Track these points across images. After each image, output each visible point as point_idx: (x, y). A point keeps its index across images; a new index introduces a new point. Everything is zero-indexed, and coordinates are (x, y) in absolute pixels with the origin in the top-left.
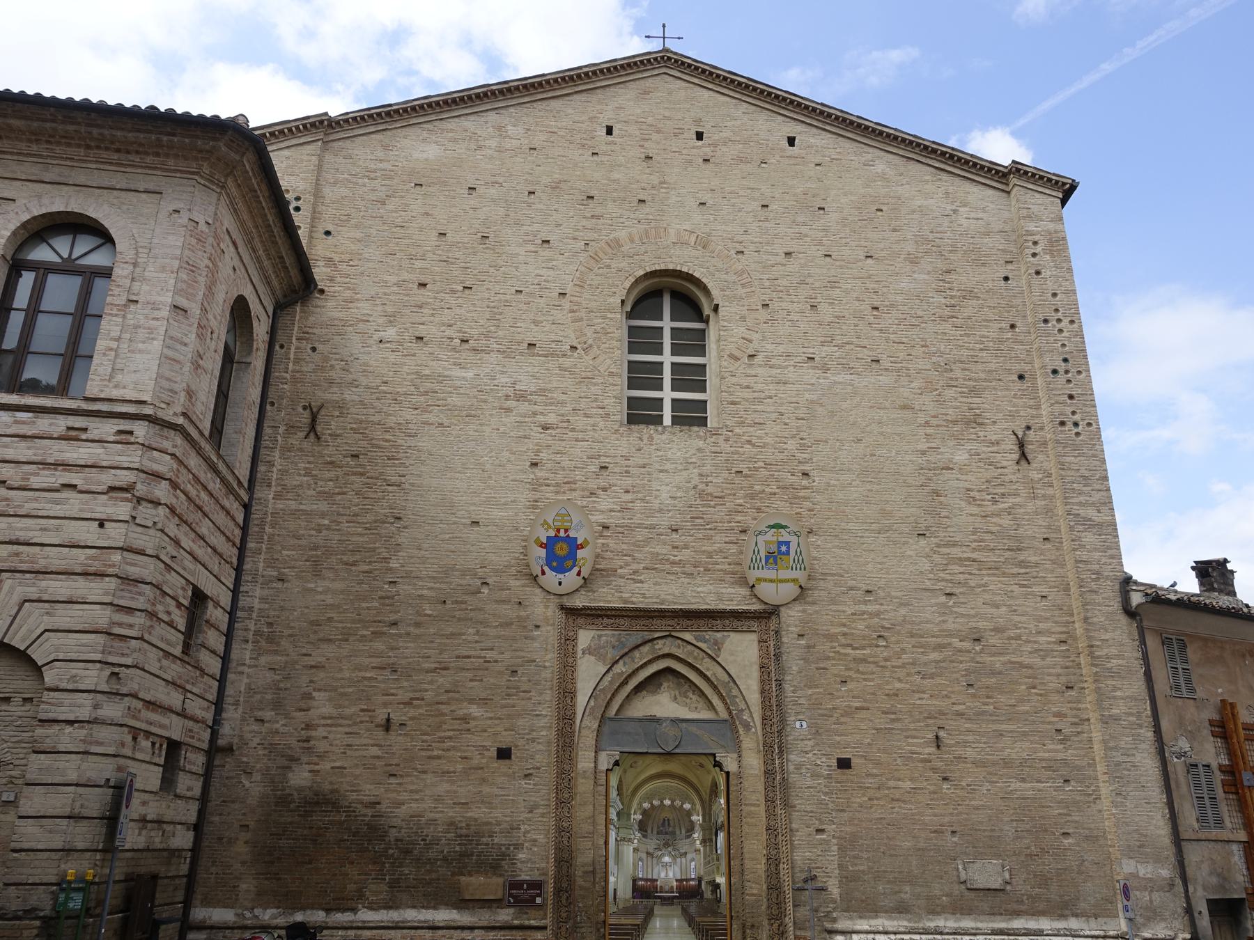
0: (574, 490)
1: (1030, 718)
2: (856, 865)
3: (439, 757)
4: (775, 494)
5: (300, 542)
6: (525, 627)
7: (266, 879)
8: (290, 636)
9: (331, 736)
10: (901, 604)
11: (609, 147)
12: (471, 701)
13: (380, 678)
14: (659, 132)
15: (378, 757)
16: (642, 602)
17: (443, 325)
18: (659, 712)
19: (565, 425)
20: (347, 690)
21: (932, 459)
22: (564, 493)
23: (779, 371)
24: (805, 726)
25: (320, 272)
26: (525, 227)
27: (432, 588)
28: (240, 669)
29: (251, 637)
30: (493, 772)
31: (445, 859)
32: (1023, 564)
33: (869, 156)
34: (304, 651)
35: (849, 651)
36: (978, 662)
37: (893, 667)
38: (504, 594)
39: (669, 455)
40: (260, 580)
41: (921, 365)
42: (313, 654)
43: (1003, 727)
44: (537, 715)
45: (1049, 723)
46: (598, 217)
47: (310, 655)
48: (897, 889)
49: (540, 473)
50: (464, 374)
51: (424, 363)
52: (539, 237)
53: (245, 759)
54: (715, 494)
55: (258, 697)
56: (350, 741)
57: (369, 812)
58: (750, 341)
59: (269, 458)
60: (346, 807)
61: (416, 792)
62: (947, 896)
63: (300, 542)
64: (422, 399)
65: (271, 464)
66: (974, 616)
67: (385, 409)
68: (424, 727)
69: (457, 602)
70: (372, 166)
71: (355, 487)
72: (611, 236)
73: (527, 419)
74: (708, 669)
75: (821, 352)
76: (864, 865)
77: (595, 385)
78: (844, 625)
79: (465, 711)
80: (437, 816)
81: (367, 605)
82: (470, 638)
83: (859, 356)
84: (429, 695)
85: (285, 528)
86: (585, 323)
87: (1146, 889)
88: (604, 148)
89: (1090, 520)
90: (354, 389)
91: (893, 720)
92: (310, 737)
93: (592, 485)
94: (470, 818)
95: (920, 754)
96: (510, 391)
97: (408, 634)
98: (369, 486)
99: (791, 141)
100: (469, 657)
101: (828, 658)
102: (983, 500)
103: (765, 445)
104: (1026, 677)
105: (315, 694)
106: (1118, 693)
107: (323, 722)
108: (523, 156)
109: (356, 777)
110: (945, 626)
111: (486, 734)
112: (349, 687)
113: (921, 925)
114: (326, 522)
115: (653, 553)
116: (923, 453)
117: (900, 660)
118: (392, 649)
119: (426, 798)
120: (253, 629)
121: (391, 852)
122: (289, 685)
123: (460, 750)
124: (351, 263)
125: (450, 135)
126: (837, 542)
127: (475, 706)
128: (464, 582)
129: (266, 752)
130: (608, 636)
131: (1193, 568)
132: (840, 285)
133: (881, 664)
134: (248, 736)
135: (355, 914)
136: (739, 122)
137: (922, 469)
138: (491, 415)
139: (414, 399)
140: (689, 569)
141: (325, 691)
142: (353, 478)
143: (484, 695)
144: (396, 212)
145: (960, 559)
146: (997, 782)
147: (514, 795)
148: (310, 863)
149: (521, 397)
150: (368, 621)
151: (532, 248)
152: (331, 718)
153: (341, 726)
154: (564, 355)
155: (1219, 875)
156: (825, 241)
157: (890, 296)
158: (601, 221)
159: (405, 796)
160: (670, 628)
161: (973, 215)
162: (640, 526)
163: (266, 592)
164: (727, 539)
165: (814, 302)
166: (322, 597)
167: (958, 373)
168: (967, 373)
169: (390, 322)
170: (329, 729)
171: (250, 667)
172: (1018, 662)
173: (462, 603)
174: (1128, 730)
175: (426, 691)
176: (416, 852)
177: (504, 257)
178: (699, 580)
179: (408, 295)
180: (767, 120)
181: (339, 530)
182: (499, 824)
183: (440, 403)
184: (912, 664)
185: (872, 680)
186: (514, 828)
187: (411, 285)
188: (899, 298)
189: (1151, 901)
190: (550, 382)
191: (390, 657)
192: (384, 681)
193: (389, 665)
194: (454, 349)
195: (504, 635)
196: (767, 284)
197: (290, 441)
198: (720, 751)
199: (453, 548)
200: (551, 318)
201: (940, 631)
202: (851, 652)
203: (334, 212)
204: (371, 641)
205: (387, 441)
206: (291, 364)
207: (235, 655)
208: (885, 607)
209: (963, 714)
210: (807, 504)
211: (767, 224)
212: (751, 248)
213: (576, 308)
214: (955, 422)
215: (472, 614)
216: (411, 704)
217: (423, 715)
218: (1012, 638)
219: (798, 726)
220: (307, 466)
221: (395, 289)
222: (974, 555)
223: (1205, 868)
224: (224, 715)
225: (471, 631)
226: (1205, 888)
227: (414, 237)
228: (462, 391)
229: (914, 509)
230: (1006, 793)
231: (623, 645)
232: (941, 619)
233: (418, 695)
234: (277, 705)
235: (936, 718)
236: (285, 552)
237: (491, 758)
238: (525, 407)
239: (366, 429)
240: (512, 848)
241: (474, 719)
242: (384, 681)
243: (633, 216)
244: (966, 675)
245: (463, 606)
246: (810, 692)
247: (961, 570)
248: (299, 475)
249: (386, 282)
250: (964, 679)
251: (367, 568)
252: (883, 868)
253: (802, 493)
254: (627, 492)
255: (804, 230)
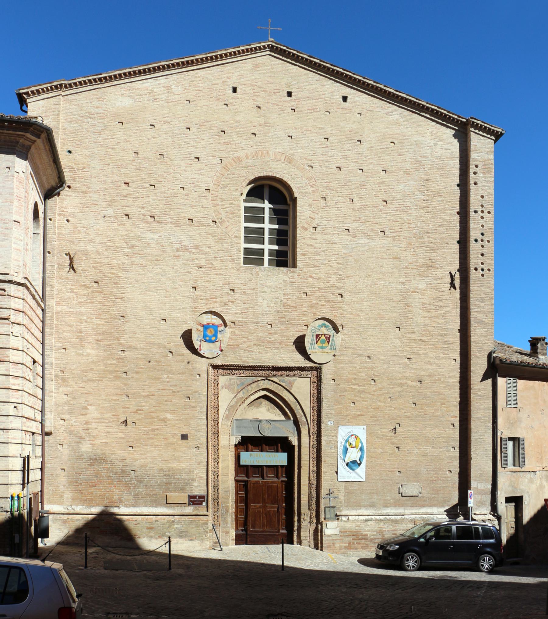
0: (216, 302)
1: (440, 419)
2: (353, 487)
3: (152, 438)
4: (323, 305)
5: (72, 329)
6: (192, 375)
7: (75, 493)
8: (73, 377)
9: (99, 428)
10: (384, 363)
11: (234, 100)
12: (167, 411)
13: (121, 399)
14: (265, 91)
15: (123, 438)
16: (252, 362)
17: (139, 207)
18: (260, 417)
19: (210, 266)
20: (104, 405)
21: (407, 287)
22: (211, 304)
23: (329, 236)
24: (333, 424)
25: (67, 175)
26: (184, 149)
27: (143, 354)
28: (51, 394)
29: (53, 378)
30: (180, 446)
31: (159, 485)
32: (446, 342)
33: (390, 109)
34: (81, 386)
35: (357, 387)
36: (419, 392)
37: (378, 395)
38: (181, 358)
39: (268, 284)
40: (54, 348)
41: (406, 234)
42: (86, 387)
43: (428, 423)
44: (200, 419)
45: (448, 421)
46: (227, 144)
47: (84, 388)
48: (370, 497)
49: (198, 293)
50: (153, 236)
51: (130, 229)
52: (192, 155)
53: (58, 438)
54: (292, 305)
55: (61, 408)
56: (109, 430)
57: (121, 464)
58: (314, 219)
59: (51, 283)
60: (110, 461)
61: (143, 454)
62: (393, 499)
63: (72, 329)
64: (130, 250)
65: (52, 286)
66: (419, 369)
67: (110, 256)
68: (144, 424)
69: (156, 361)
70: (92, 110)
71: (98, 299)
72: (236, 155)
73: (189, 262)
74: (286, 396)
75: (352, 226)
76: (356, 487)
77: (226, 243)
78: (355, 374)
79: (164, 416)
80: (154, 465)
81: (110, 362)
82: (164, 380)
83: (374, 228)
84: (146, 408)
85: (63, 321)
86: (220, 207)
87: (480, 494)
88: (231, 101)
89: (482, 320)
90: (92, 244)
91: (376, 420)
92: (89, 428)
93: (225, 299)
94: (170, 467)
95: (387, 436)
96: (179, 246)
97: (133, 377)
98: (106, 299)
99: (345, 99)
100: (164, 390)
101: (346, 391)
102: (430, 309)
103: (319, 278)
104: (441, 399)
105: (88, 407)
106: (482, 407)
107: (94, 421)
108: (182, 105)
109: (113, 447)
110: (405, 374)
111: (175, 427)
112: (105, 403)
113: (380, 512)
114: (85, 318)
115: (258, 336)
116: (403, 283)
117: (381, 392)
118: (126, 385)
119: (148, 457)
120: (54, 374)
121: (133, 482)
122: (75, 403)
123: (163, 435)
124: (84, 170)
125: (138, 91)
126: (354, 331)
127: (169, 414)
128: (159, 351)
129: (68, 435)
130: (235, 380)
131: (529, 341)
132: (366, 187)
133: (372, 393)
134: (58, 427)
135: (119, 509)
136: (314, 86)
137: (401, 292)
138: (169, 260)
139: (126, 250)
140: (277, 345)
141: (94, 405)
142: (97, 294)
143: (173, 409)
144: (108, 139)
145: (416, 340)
146: (422, 449)
147: (190, 456)
148: (95, 486)
149: (185, 250)
150: (111, 371)
151: (189, 162)
152: (98, 419)
153: (103, 423)
154: (209, 226)
155: (513, 487)
156: (360, 161)
157: (394, 194)
158: (229, 146)
159: (137, 457)
160: (267, 376)
161: (445, 147)
162: (251, 322)
163: (58, 355)
164: (297, 330)
165: (351, 197)
166: (86, 358)
167: (426, 239)
168: (430, 239)
169: (110, 205)
170: (97, 424)
171: (55, 393)
172: (437, 392)
173: (159, 362)
174: (483, 424)
175: (144, 406)
176: (145, 482)
177: (173, 167)
178: (282, 351)
179: (118, 189)
180: (330, 85)
181: (92, 322)
182: (183, 469)
183: (141, 252)
184: (387, 393)
185: (367, 401)
186: (191, 471)
187: (119, 184)
188: (398, 196)
189: (481, 499)
190: (201, 242)
191: (124, 389)
192: (122, 401)
193: (124, 393)
194: (146, 222)
195: (181, 379)
196: (325, 185)
197: (61, 273)
198: (291, 435)
199: (152, 333)
200: (200, 204)
201: (402, 377)
202: (358, 387)
203: (72, 139)
204: (114, 381)
205: (113, 274)
206: (56, 230)
207: (47, 387)
208: (376, 365)
209: (409, 417)
210: (340, 311)
211: (326, 150)
212: (317, 164)
213: (215, 198)
214: (421, 267)
215: (165, 368)
216: (137, 412)
217: (143, 418)
218: (437, 380)
219: (329, 424)
220: (71, 287)
221: (111, 186)
222: (423, 338)
223: (507, 484)
224: (46, 417)
225: (165, 376)
226: (505, 493)
227: (120, 154)
228: (152, 246)
229: (395, 314)
230: (425, 454)
231: (243, 384)
232: (403, 371)
233: (140, 408)
234: (71, 412)
235: (396, 419)
236: (65, 334)
237: (178, 439)
238: (187, 255)
239: (100, 267)
240: (190, 480)
241: (169, 420)
242: (122, 401)
243: (248, 143)
244: (413, 398)
245: (160, 363)
246: (336, 407)
247: (416, 345)
248: (68, 292)
249: (105, 181)
250: (411, 400)
251: (108, 343)
252: (365, 488)
253: (338, 305)
254: (244, 303)
255: (348, 153)
